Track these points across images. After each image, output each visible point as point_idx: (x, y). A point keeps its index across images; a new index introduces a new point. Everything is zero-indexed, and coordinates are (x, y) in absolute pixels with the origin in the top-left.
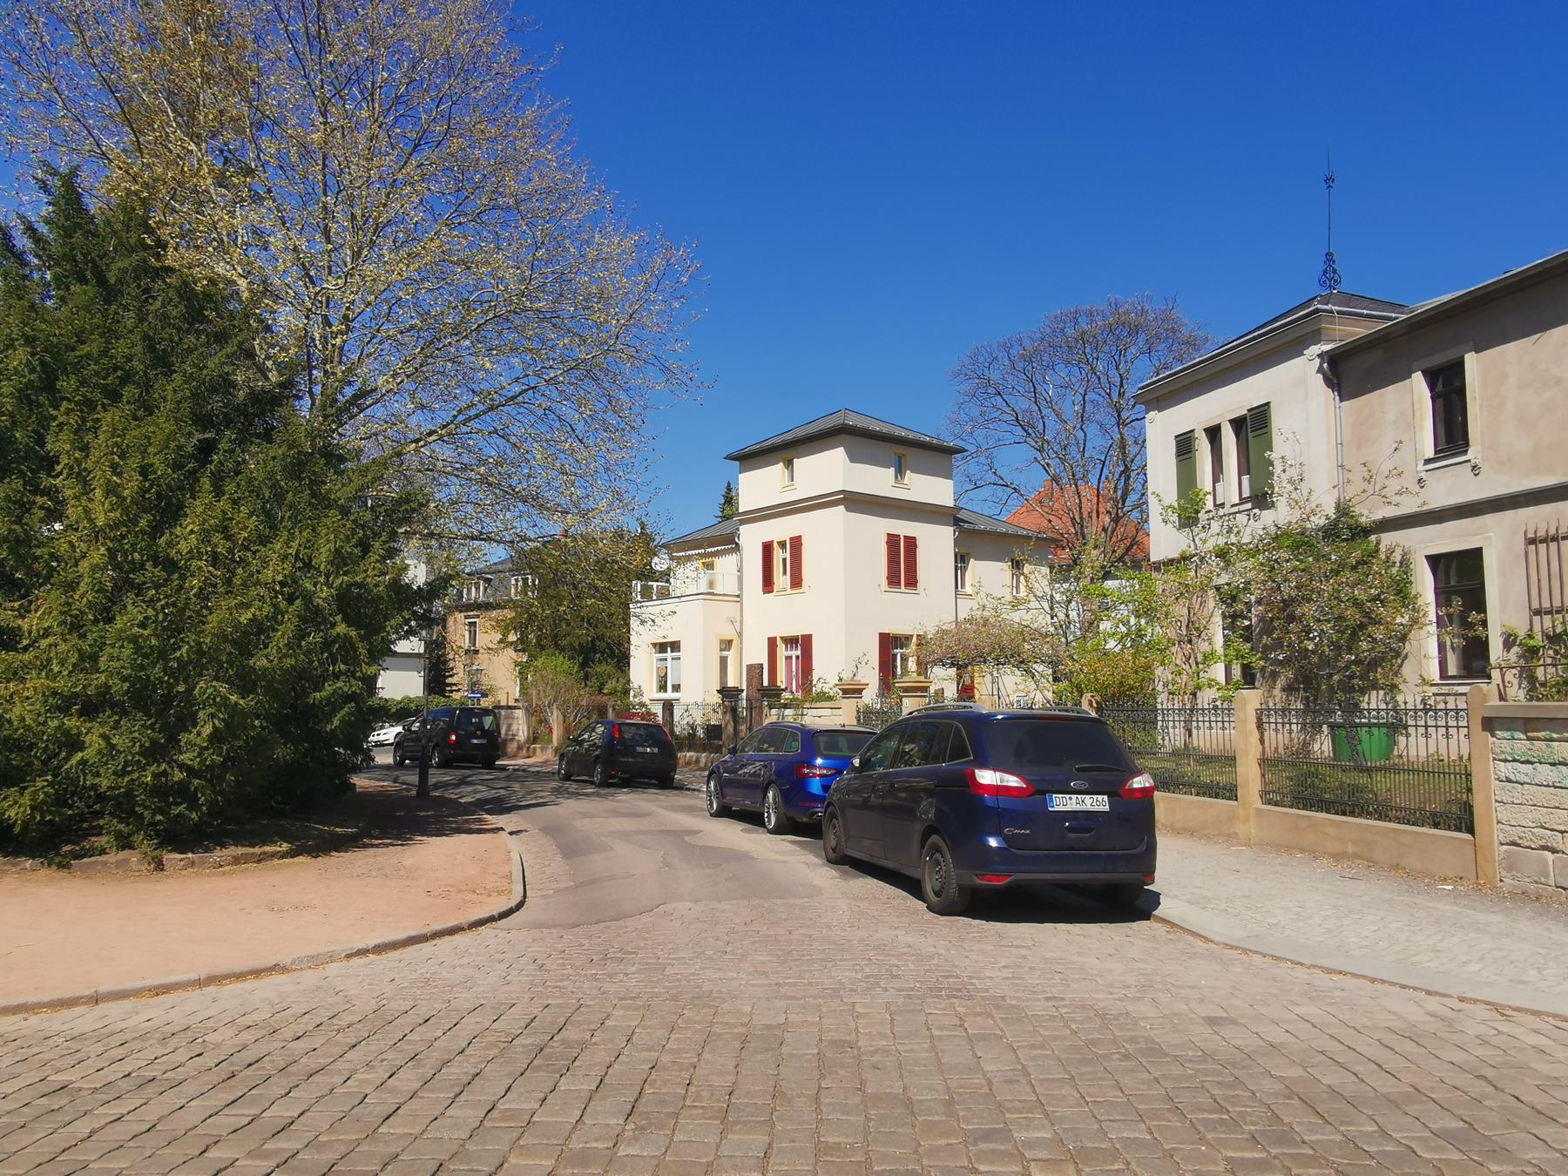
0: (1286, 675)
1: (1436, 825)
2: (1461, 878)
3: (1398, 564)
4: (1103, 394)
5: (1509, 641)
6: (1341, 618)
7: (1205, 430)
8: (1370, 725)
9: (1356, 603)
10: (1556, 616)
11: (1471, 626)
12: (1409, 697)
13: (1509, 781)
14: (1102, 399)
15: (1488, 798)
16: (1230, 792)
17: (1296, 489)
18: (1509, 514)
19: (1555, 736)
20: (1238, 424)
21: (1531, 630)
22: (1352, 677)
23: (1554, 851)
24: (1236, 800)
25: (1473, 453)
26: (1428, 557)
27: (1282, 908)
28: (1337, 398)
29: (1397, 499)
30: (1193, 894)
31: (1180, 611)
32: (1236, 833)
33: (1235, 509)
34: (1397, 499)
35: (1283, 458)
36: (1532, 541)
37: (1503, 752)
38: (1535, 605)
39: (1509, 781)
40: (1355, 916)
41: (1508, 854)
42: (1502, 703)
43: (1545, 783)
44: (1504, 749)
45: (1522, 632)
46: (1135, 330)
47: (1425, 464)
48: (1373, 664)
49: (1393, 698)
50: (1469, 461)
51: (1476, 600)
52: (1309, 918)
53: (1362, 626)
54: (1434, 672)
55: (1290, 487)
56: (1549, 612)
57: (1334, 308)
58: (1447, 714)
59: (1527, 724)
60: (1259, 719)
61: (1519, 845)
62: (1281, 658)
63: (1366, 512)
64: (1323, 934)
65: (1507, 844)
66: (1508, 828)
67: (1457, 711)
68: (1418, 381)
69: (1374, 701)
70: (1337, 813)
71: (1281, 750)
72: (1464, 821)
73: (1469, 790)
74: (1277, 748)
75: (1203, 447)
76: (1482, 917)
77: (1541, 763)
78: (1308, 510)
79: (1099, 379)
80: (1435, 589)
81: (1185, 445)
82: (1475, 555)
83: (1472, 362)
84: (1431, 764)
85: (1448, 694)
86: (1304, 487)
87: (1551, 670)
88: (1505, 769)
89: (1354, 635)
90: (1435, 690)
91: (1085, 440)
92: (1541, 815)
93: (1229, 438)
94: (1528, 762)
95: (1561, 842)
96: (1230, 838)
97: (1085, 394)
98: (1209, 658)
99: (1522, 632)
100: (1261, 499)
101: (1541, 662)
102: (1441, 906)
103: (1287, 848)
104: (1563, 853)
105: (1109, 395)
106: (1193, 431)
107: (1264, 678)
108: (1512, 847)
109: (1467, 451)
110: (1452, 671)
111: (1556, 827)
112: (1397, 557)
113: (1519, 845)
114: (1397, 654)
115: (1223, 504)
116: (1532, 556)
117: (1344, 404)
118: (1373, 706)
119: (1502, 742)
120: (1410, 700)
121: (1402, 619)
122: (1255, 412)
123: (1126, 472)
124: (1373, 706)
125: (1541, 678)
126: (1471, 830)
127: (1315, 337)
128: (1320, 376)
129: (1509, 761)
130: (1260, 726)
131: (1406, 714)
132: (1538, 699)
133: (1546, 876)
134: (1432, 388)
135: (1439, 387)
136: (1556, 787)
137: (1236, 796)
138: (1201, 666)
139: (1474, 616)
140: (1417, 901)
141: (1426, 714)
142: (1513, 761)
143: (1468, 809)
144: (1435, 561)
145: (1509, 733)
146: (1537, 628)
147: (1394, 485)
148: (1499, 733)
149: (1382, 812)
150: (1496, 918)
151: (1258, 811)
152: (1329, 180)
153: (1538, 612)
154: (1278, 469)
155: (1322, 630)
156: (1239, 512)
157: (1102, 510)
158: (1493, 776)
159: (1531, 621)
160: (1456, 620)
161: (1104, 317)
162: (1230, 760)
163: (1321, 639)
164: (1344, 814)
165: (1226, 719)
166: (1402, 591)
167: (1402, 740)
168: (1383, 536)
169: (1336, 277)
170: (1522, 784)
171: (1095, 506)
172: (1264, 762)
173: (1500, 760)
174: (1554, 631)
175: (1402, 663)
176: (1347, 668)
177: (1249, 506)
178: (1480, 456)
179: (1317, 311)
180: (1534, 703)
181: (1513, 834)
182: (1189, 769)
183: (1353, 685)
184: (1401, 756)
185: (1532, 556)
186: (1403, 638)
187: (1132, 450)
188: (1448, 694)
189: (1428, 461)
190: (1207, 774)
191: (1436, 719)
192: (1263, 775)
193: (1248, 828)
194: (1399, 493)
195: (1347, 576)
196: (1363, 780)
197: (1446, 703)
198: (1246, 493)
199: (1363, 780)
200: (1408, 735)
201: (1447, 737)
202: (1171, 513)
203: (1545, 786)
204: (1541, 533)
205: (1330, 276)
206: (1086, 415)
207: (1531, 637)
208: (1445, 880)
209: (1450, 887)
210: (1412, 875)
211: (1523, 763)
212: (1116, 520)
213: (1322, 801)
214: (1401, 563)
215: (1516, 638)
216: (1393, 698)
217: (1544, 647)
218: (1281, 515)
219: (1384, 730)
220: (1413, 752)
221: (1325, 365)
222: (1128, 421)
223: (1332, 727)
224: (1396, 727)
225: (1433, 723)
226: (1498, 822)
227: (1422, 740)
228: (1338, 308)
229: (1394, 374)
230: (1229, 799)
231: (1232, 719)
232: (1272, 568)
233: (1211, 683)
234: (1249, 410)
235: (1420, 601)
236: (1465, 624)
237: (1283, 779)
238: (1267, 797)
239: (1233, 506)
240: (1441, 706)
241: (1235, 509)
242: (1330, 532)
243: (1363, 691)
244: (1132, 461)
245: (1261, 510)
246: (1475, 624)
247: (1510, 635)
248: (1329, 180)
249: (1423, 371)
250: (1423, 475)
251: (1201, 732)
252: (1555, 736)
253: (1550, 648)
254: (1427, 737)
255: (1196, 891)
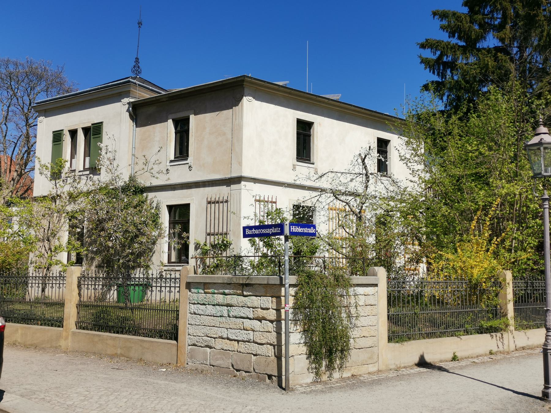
0: (98, 259)
1: (161, 337)
2: (170, 364)
3: (155, 208)
4: (20, 109)
5: (197, 247)
6: (127, 231)
7: (69, 131)
8: (135, 285)
9: (135, 225)
10: (216, 236)
11: (183, 238)
12: (154, 271)
13: (195, 314)
14: (18, 111)
15: (185, 322)
16: (59, 323)
17: (111, 164)
18: (202, 189)
19: (216, 291)
20: (86, 130)
21: (206, 242)
22: (128, 261)
23: (211, 347)
24: (63, 327)
25: (190, 160)
26: (168, 206)
27: (77, 393)
28: (135, 126)
29: (157, 175)
30: (26, 389)
31: (45, 223)
32: (60, 346)
33: (81, 173)
34: (157, 175)
35: (107, 146)
36: (209, 203)
37: (194, 300)
38: (208, 231)
39: (195, 314)
40: (116, 394)
41: (192, 351)
42: (195, 275)
43: (210, 314)
44: (194, 298)
45: (202, 243)
46: (40, 78)
47: (170, 163)
48: (140, 255)
49: (147, 272)
50: (188, 163)
51: (186, 228)
52: (92, 398)
53: (136, 236)
54: (165, 261)
55: (108, 162)
56: (213, 235)
57: (137, 82)
58: (171, 280)
59: (205, 286)
60: (79, 282)
61: (196, 345)
62: (95, 250)
63: (143, 182)
64: (97, 408)
65: (192, 345)
66: (192, 337)
67: (175, 279)
68: (170, 122)
69: (138, 273)
70: (114, 333)
71: (93, 298)
72: (174, 334)
73: (177, 319)
74: (90, 298)
75: (67, 139)
76: (178, 386)
77: (209, 305)
78: (116, 175)
79: (17, 99)
80: (169, 221)
81: (57, 137)
82: (187, 206)
83: (192, 118)
84: (171, 307)
85: (172, 271)
86: (115, 164)
87: (212, 260)
88: (193, 308)
89: (132, 240)
90: (166, 268)
91: (7, 131)
92: (207, 330)
93: (81, 137)
94: (204, 304)
95: (214, 343)
96: (56, 349)
97: (9, 107)
98: (58, 249)
99: (202, 243)
100: (94, 170)
101: (209, 256)
102: (159, 382)
103: (85, 353)
104: (214, 348)
105: (23, 109)
106: (62, 130)
107: (87, 260)
108: (193, 347)
109: (187, 159)
110: (173, 259)
111: (212, 336)
112: (154, 205)
113: (196, 345)
114: (151, 250)
115: (75, 170)
116: (209, 209)
117: (138, 129)
118: (137, 276)
119: (198, 295)
120: (155, 273)
121: (155, 233)
122: (95, 125)
123: (28, 152)
124: (137, 276)
125: (208, 264)
126: (176, 339)
127: (127, 94)
128: (128, 114)
129: (196, 304)
130: (79, 286)
131: (152, 280)
132: (206, 274)
133: (206, 360)
134: (176, 128)
135: (179, 129)
136: (214, 316)
137: (63, 325)
138: (53, 253)
139: (184, 234)
140: (149, 380)
141: (161, 280)
142: (197, 304)
143: (176, 328)
144: (170, 208)
145: (197, 290)
146: (208, 242)
147: (156, 168)
148: (193, 290)
149: (135, 331)
150: (184, 386)
151: (74, 333)
152: (140, 24)
153: (209, 234)
154: (103, 152)
155: (117, 237)
156: (83, 175)
157: (13, 169)
158: (188, 311)
159: (206, 238)
160: (177, 235)
161: (24, 68)
162: (61, 304)
163: (116, 241)
164: (118, 333)
165: (61, 282)
166: (155, 219)
167: (149, 293)
168: (149, 194)
169: (139, 70)
170: (200, 315)
171: (9, 167)
172: (81, 305)
173: (192, 304)
174: (214, 243)
175: (152, 255)
176: (127, 256)
177: (88, 172)
178: (192, 161)
179: (129, 81)
180: (204, 275)
181: (194, 340)
182: (39, 311)
183: (129, 265)
184: (148, 300)
185: (209, 209)
186: (154, 243)
187: (32, 140)
188: (172, 271)
189: (171, 161)
190: (50, 313)
191: (165, 283)
192: (78, 313)
193: (67, 343)
194: (158, 173)
195: (131, 210)
196: (128, 314)
197: (171, 275)
198: (87, 166)
199: (128, 314)
200: (152, 291)
201: (170, 292)
202: (44, 170)
203: (210, 316)
204: (213, 200)
205: (137, 69)
206: (8, 117)
207: (205, 245)
208: (162, 365)
209: (164, 370)
210: (147, 364)
211: (201, 304)
212: (20, 175)
213: (107, 326)
214: (156, 208)
215: (200, 245)
216: (147, 272)
217: (210, 250)
218: (104, 177)
219: (141, 288)
220: (154, 298)
221: (131, 109)
222: (32, 125)
223: (119, 286)
224: (146, 286)
225: (174, 285)
226: (189, 334)
227: (158, 293)
228: (139, 83)
229: (159, 119)
230: (59, 326)
231: (65, 282)
232: (96, 203)
233: (58, 262)
234: (92, 124)
235: (163, 226)
236: (180, 237)
237: (88, 314)
238: (80, 325)
239: (80, 172)
240: (168, 276)
241: (81, 173)
242: (125, 189)
243: (133, 268)
244: (32, 146)
245: (94, 175)
246: (184, 238)
247: (198, 244)
248: (140, 24)
249: (173, 120)
250: (169, 167)
251: (33, 289)
252: (216, 291)
253: (212, 250)
254: (161, 292)
255: (27, 387)
